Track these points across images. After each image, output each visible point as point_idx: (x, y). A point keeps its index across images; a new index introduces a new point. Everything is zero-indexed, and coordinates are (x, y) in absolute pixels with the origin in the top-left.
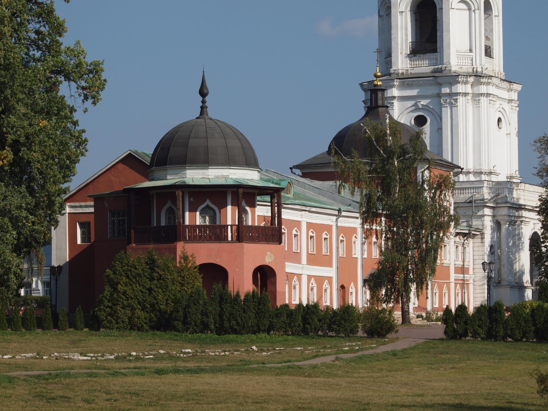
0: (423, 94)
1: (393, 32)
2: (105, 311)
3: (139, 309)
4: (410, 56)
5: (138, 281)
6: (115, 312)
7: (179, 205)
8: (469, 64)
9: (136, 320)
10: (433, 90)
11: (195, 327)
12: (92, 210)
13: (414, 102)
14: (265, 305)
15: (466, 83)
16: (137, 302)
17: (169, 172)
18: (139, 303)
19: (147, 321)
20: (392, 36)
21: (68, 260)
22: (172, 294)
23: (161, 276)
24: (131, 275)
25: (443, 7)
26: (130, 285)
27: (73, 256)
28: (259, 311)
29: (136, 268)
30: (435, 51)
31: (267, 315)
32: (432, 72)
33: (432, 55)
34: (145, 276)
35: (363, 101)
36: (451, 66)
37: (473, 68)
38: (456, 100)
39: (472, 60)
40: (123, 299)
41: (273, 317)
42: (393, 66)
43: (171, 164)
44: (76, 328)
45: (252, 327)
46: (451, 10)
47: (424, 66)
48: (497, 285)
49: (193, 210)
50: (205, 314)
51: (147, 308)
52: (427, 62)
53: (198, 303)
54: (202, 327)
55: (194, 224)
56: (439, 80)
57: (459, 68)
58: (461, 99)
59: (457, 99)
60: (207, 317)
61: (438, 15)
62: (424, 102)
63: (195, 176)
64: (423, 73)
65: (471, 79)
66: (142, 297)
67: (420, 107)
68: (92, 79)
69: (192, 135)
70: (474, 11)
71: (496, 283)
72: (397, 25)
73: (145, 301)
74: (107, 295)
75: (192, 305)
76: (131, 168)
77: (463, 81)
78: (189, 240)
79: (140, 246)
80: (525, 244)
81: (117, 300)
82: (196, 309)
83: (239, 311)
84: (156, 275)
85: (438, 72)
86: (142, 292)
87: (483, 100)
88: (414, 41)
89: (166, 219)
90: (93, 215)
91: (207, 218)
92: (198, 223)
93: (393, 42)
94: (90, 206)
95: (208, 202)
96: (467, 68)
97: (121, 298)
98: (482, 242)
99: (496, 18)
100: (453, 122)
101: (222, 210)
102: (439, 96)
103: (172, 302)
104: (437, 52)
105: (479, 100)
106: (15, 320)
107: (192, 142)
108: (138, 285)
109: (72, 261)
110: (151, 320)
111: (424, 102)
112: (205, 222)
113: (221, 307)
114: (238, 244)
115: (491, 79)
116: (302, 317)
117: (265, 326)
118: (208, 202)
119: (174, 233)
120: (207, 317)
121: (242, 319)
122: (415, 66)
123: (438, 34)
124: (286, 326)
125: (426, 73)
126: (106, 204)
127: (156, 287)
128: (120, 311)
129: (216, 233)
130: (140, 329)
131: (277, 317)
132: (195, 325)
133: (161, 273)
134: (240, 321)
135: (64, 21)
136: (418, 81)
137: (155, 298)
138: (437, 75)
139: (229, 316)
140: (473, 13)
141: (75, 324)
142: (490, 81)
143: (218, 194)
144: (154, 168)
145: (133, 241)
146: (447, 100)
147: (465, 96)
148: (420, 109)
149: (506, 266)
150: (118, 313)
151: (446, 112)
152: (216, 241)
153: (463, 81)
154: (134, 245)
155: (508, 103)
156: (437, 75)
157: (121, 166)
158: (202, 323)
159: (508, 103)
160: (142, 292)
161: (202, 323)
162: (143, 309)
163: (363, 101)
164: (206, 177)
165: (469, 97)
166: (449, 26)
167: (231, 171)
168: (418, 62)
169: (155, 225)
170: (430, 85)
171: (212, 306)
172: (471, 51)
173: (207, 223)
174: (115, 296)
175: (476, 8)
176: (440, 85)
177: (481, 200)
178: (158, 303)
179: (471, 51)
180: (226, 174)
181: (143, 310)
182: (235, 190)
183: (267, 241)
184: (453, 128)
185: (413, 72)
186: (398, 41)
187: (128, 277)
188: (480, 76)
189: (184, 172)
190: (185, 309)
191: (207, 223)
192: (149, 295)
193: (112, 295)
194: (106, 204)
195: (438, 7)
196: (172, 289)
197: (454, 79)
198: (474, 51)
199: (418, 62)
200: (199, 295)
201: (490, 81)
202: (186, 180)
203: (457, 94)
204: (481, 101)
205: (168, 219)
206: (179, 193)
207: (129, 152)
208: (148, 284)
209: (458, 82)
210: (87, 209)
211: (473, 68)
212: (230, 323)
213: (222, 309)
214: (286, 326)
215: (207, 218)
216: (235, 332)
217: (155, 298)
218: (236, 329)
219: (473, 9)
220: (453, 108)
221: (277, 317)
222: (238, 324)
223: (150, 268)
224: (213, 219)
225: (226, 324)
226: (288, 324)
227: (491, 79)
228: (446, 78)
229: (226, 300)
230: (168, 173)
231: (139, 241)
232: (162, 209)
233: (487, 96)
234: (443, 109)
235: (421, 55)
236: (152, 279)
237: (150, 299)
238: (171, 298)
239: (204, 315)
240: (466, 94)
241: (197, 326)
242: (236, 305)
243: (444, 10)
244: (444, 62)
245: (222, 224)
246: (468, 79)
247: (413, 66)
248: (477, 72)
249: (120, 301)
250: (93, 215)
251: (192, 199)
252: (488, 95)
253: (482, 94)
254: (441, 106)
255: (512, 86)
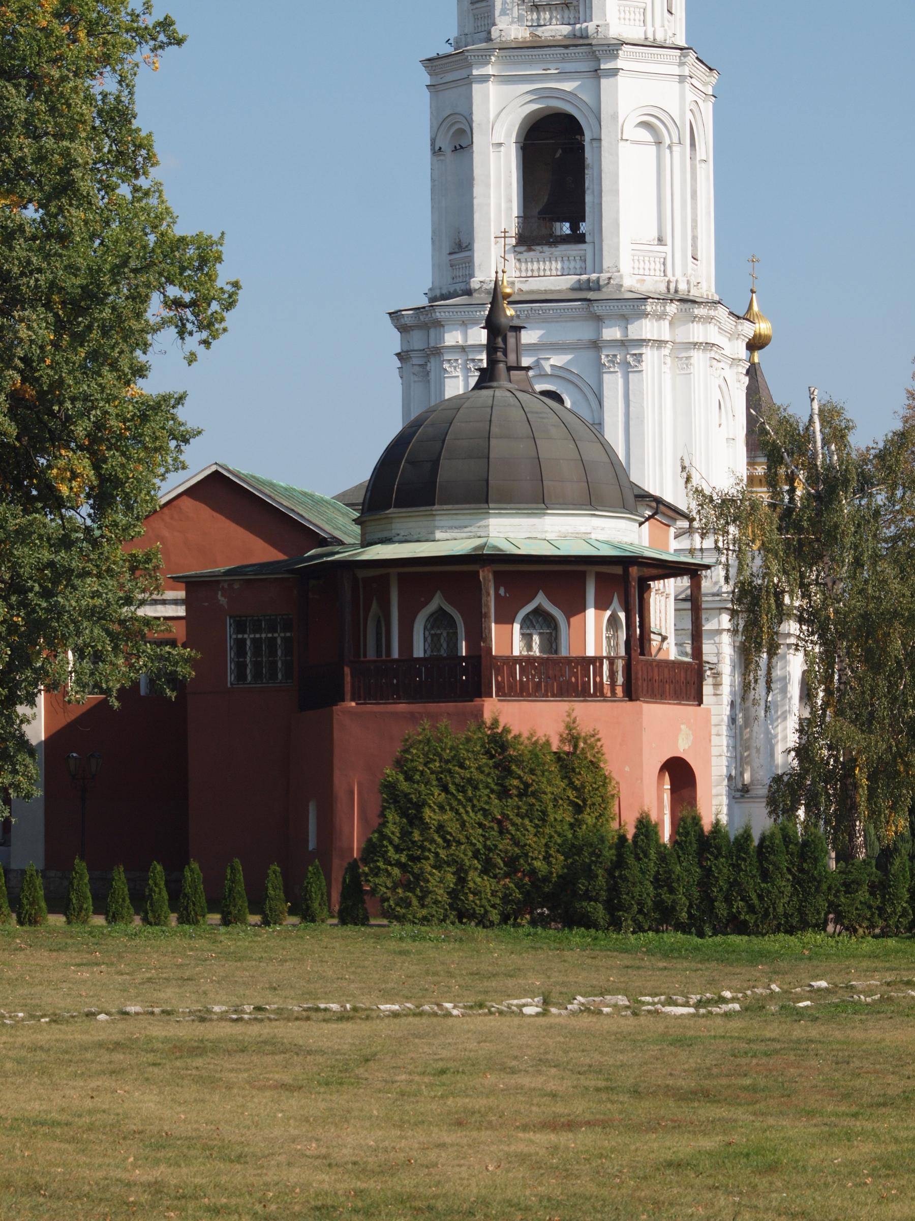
0: (554, 340)
1: (478, 190)
2: (389, 875)
3: (476, 869)
4: (517, 249)
5: (470, 800)
6: (419, 877)
7: (488, 607)
8: (658, 273)
9: (471, 897)
10: (582, 332)
11: (640, 918)
12: (181, 611)
13: (535, 358)
14: (816, 860)
15: (661, 317)
16: (470, 854)
17: (441, 521)
18: (476, 854)
19: (498, 902)
20: (476, 202)
21: (43, 739)
22: (556, 832)
23: (527, 785)
24: (454, 783)
25: (603, 138)
26: (452, 809)
27: (54, 730)
28: (805, 877)
29: (462, 766)
30: (578, 238)
31: (824, 887)
32: (573, 289)
33: (572, 250)
34: (487, 787)
35: (398, 355)
36: (621, 277)
37: (669, 282)
38: (639, 357)
39: (664, 264)
40: (438, 845)
41: (838, 891)
42: (477, 273)
43: (442, 503)
44: (308, 916)
45: (786, 915)
46: (621, 144)
47: (550, 274)
48: (742, 796)
49: (506, 618)
50: (663, 881)
51: (495, 866)
52: (559, 266)
53: (646, 855)
54: (657, 916)
55: (507, 654)
56: (598, 309)
57: (638, 281)
58: (649, 355)
59: (641, 354)
60: (672, 891)
61: (588, 154)
62: (558, 360)
63: (514, 532)
64: (552, 292)
65: (672, 308)
66: (481, 839)
67: (548, 370)
68: (194, 281)
69: (495, 430)
70: (670, 147)
71: (738, 790)
72: (489, 176)
73: (490, 850)
74: (393, 833)
75: (631, 861)
76: (213, 508)
77: (656, 311)
78: (595, 695)
79: (369, 708)
80: (793, 702)
81: (423, 848)
82: (643, 872)
83: (753, 877)
84: (516, 782)
85: (590, 289)
86: (481, 825)
87: (698, 357)
88: (522, 215)
89: (425, 639)
90: (184, 622)
91: (536, 639)
92: (516, 653)
93: (476, 216)
94: (175, 602)
95: (541, 600)
96: (653, 284)
97: (433, 841)
98: (715, 695)
99: (703, 165)
100: (631, 409)
101: (572, 620)
102: (596, 345)
103: (558, 851)
104: (584, 242)
105: (688, 358)
106: (155, 897)
107: (498, 448)
108: (469, 809)
109: (46, 741)
110: (506, 899)
111: (558, 360)
112: (530, 648)
113: (701, 867)
114: (630, 704)
115: (716, 309)
116: (908, 890)
117: (819, 913)
118: (541, 600)
119: (467, 677)
120: (672, 891)
121: (760, 897)
122: (530, 274)
123: (588, 199)
124: (873, 914)
125: (559, 291)
126: (222, 600)
127: (517, 815)
128: (432, 874)
129: (563, 676)
130: (483, 922)
131: (846, 892)
132: (640, 911)
133: (528, 778)
134: (755, 901)
135: (150, 135)
136: (545, 311)
137: (516, 843)
138: (591, 295)
139: (729, 890)
140: (668, 151)
141: (308, 908)
142: (712, 313)
143: (565, 579)
144: (392, 510)
145: (348, 695)
146: (615, 356)
147: (659, 347)
148: (547, 375)
149: (762, 749)
150: (428, 881)
151: (613, 384)
152: (561, 695)
153: (656, 311)
154: (353, 704)
155: (731, 366)
156: (591, 295)
157: (187, 502)
158: (659, 905)
159: (731, 366)
160: (481, 825)
161: (659, 905)
162: (487, 868)
163: (398, 355)
164: (539, 536)
165: (666, 351)
166: (616, 182)
167: (596, 521)
168: (535, 266)
169: (395, 654)
170: (573, 319)
171: (680, 863)
172: (661, 241)
173: (536, 651)
174: (416, 836)
175: (676, 140)
176: (598, 320)
177: (714, 595)
178: (526, 855)
179: (661, 241)
180: (583, 529)
181: (485, 871)
182: (618, 570)
183: (677, 698)
184: (631, 423)
185: (525, 287)
186: (488, 213)
187: (445, 789)
188: (694, 302)
189: (483, 523)
190: (610, 873)
191: (536, 651)
192: (501, 832)
193: (405, 834)
194: (222, 600)
195: (588, 136)
196: (555, 820)
197: (634, 306)
198: (669, 242)
199: (535, 266)
200: (646, 836)
201: (712, 313)
202: (493, 541)
203: (642, 342)
204: (692, 361)
205: (433, 641)
206: (486, 575)
207: (214, 468)
208: (495, 806)
209: (645, 315)
210: (159, 607)
211: (669, 282)
212: (731, 906)
213: (708, 872)
214: (873, 914)
215: (536, 639)
216: (742, 928)
217: (516, 843)
218: (745, 922)
219: (667, 142)
220: (631, 375)
221: (846, 892)
222: (751, 909)
223: (496, 766)
224: (551, 641)
225: (721, 909)
226: (878, 908)
227: (716, 309)
228: (615, 304)
229: (719, 849)
230: (437, 523)
231: (363, 695)
232: (415, 617)
233: (705, 350)
234: (606, 377)
235: (546, 248)
236: (504, 793)
237: (505, 844)
238: (555, 843)
239: (661, 887)
240: (659, 343)
241: (645, 915)
242: (744, 860)
243: (604, 143)
244: (605, 266)
245: (574, 653)
246: (667, 308)
247: (524, 274)
248: (676, 291)
249: (429, 850)
250: (184, 622)
251: (502, 591)
252: (709, 346)
253: (695, 345)
254: (600, 369)
255: (740, 328)
